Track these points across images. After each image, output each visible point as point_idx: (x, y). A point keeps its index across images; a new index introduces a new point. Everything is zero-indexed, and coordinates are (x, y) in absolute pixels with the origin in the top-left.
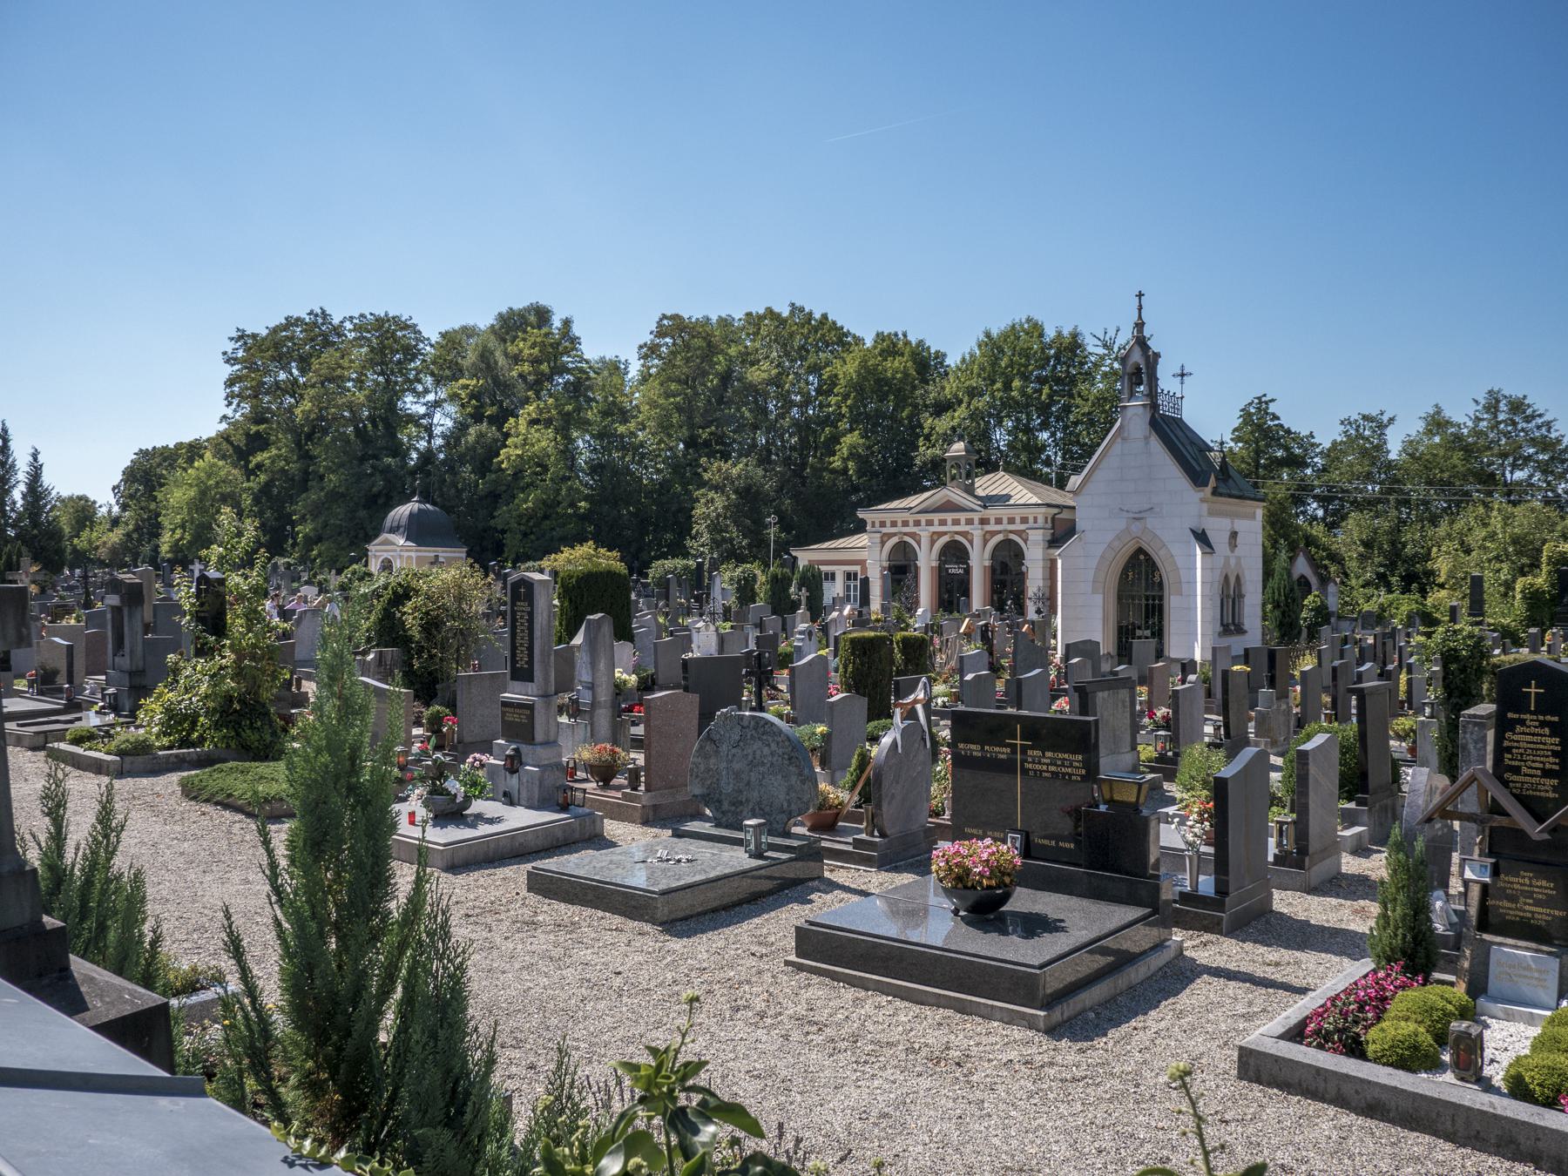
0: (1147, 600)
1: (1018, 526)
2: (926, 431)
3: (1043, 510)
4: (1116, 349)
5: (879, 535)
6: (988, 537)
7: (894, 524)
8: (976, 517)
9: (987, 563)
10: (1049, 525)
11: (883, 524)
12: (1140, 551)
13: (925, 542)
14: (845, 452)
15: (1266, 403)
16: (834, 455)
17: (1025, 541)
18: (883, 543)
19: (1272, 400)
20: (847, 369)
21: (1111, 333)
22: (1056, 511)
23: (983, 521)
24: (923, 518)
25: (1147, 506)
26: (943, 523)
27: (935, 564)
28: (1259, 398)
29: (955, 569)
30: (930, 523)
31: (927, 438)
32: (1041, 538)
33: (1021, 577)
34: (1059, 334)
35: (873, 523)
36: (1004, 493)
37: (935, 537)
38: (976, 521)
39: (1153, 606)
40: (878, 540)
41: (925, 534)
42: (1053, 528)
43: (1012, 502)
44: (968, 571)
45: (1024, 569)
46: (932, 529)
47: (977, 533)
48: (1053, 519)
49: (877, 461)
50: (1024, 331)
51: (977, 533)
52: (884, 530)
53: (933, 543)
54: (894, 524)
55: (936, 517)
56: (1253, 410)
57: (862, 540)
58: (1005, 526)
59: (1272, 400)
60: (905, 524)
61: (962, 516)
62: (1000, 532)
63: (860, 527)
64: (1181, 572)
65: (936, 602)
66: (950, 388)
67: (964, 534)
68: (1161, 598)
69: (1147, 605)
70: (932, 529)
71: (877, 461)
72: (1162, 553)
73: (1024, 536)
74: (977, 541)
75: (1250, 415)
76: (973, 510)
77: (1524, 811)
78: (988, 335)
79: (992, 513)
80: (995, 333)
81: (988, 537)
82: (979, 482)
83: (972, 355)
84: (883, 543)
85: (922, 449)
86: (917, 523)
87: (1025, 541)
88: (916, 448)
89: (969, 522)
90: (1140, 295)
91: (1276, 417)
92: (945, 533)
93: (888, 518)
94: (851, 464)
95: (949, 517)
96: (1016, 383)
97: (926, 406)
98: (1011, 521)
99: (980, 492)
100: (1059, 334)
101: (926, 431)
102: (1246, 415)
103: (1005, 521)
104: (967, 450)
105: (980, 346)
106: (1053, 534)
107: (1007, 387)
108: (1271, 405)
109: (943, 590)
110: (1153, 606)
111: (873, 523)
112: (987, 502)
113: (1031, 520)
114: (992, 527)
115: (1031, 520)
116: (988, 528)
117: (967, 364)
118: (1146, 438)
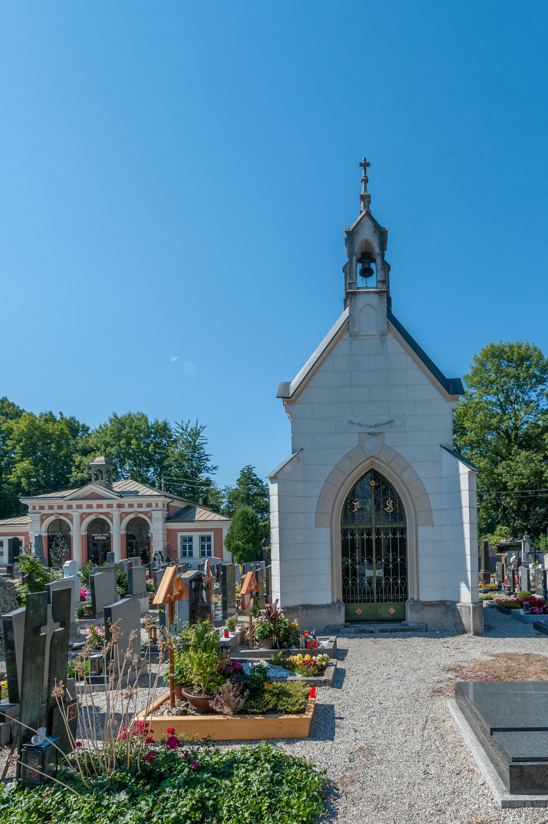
0: (394, 534)
1: (145, 509)
2: (77, 464)
3: (162, 499)
4: (189, 430)
5: (39, 515)
6: (123, 515)
7: (51, 508)
8: (114, 503)
9: (124, 532)
10: (166, 509)
11: (42, 508)
12: (375, 474)
13: (76, 519)
14: (19, 473)
15: (251, 468)
16: (11, 474)
17: (150, 518)
18: (42, 521)
19: (254, 468)
20: (22, 425)
21: (186, 422)
22: (170, 500)
23: (120, 506)
24: (74, 503)
25: (386, 419)
26: (90, 506)
27: (84, 533)
28: (248, 467)
29: (99, 537)
30: (79, 507)
31: (78, 467)
32: (161, 516)
33: (148, 542)
34: (157, 422)
35: (34, 508)
36: (134, 490)
37: (84, 516)
38: (115, 506)
39: (395, 540)
40: (39, 519)
41: (76, 514)
42: (168, 510)
43: (139, 494)
44: (109, 538)
45: (150, 535)
46: (81, 511)
47: (115, 513)
48: (168, 505)
49: (43, 479)
50: (136, 418)
51: (115, 513)
52: (43, 512)
53: (82, 520)
54: (51, 508)
55: (84, 503)
56: (246, 472)
57: (27, 519)
58: (135, 509)
59: (254, 468)
60: (60, 507)
61: (104, 503)
62: (132, 513)
63: (23, 511)
64: (430, 496)
65: (85, 557)
66: (92, 442)
67: (106, 514)
68: (403, 531)
69: (378, 541)
70: (81, 511)
71: (43, 479)
72: (406, 475)
73: (149, 515)
74: (116, 519)
75: (244, 473)
76: (112, 499)
77: (371, 634)
78: (115, 416)
79: (126, 501)
80: (119, 416)
81: (123, 515)
82: (114, 484)
83: (105, 426)
84: (42, 521)
85: (74, 474)
86: (70, 507)
87: (150, 518)
88: (71, 472)
89: (110, 506)
90: (365, 165)
91: (255, 475)
92: (92, 514)
93: (46, 503)
94: (23, 480)
95: (94, 503)
96: (133, 441)
97: (77, 451)
98: (140, 506)
99: (116, 489)
100: (157, 422)
101: (77, 464)
102: (243, 474)
103: (135, 506)
104: (106, 461)
105: (110, 421)
106: (168, 514)
107: (129, 443)
108: (253, 469)
109: (91, 552)
110: (395, 540)
111: (34, 508)
112: (121, 495)
113: (154, 505)
114: (126, 509)
115: (154, 505)
116: (123, 510)
117: (102, 431)
118: (383, 335)
